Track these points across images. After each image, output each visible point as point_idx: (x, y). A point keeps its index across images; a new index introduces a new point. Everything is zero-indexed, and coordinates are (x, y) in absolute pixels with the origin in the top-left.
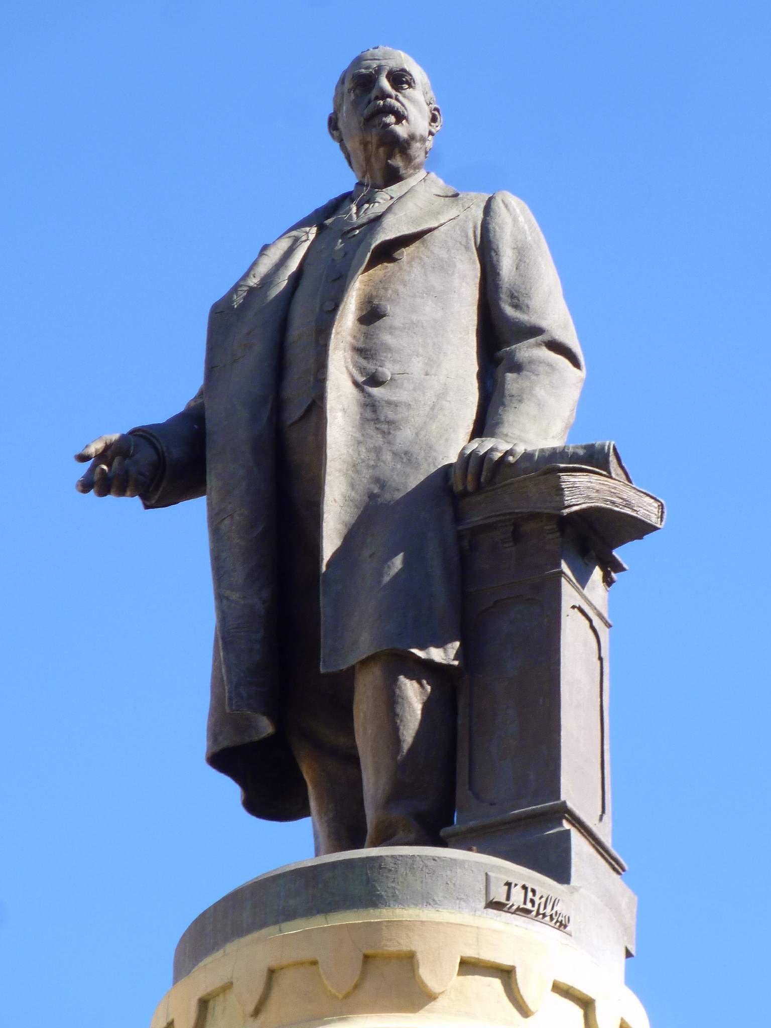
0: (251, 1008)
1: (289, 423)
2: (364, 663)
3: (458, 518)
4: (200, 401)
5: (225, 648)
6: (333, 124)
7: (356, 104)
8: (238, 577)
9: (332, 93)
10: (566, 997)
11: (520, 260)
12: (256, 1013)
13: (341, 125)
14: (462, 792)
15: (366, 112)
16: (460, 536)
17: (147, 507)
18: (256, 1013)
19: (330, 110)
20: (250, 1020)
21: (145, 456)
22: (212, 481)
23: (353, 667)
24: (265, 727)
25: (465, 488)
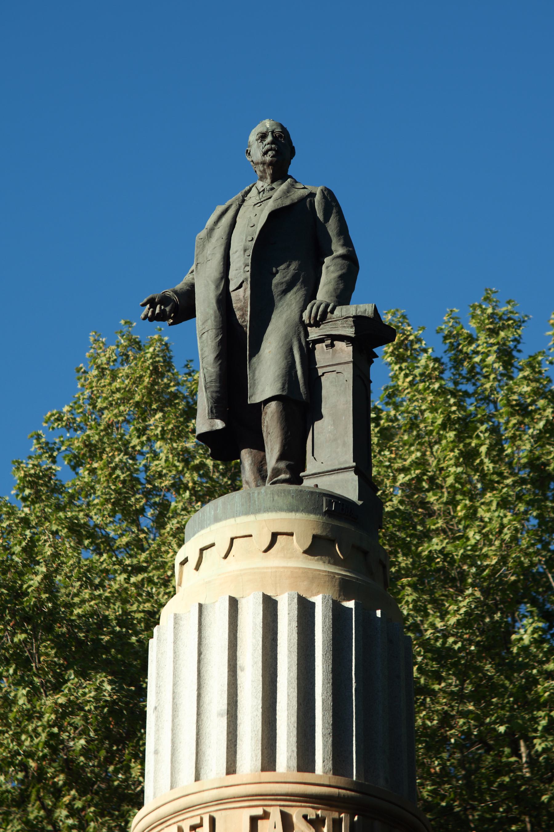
0: (223, 555)
15: (264, 150)
16: (307, 343)
18: (226, 557)
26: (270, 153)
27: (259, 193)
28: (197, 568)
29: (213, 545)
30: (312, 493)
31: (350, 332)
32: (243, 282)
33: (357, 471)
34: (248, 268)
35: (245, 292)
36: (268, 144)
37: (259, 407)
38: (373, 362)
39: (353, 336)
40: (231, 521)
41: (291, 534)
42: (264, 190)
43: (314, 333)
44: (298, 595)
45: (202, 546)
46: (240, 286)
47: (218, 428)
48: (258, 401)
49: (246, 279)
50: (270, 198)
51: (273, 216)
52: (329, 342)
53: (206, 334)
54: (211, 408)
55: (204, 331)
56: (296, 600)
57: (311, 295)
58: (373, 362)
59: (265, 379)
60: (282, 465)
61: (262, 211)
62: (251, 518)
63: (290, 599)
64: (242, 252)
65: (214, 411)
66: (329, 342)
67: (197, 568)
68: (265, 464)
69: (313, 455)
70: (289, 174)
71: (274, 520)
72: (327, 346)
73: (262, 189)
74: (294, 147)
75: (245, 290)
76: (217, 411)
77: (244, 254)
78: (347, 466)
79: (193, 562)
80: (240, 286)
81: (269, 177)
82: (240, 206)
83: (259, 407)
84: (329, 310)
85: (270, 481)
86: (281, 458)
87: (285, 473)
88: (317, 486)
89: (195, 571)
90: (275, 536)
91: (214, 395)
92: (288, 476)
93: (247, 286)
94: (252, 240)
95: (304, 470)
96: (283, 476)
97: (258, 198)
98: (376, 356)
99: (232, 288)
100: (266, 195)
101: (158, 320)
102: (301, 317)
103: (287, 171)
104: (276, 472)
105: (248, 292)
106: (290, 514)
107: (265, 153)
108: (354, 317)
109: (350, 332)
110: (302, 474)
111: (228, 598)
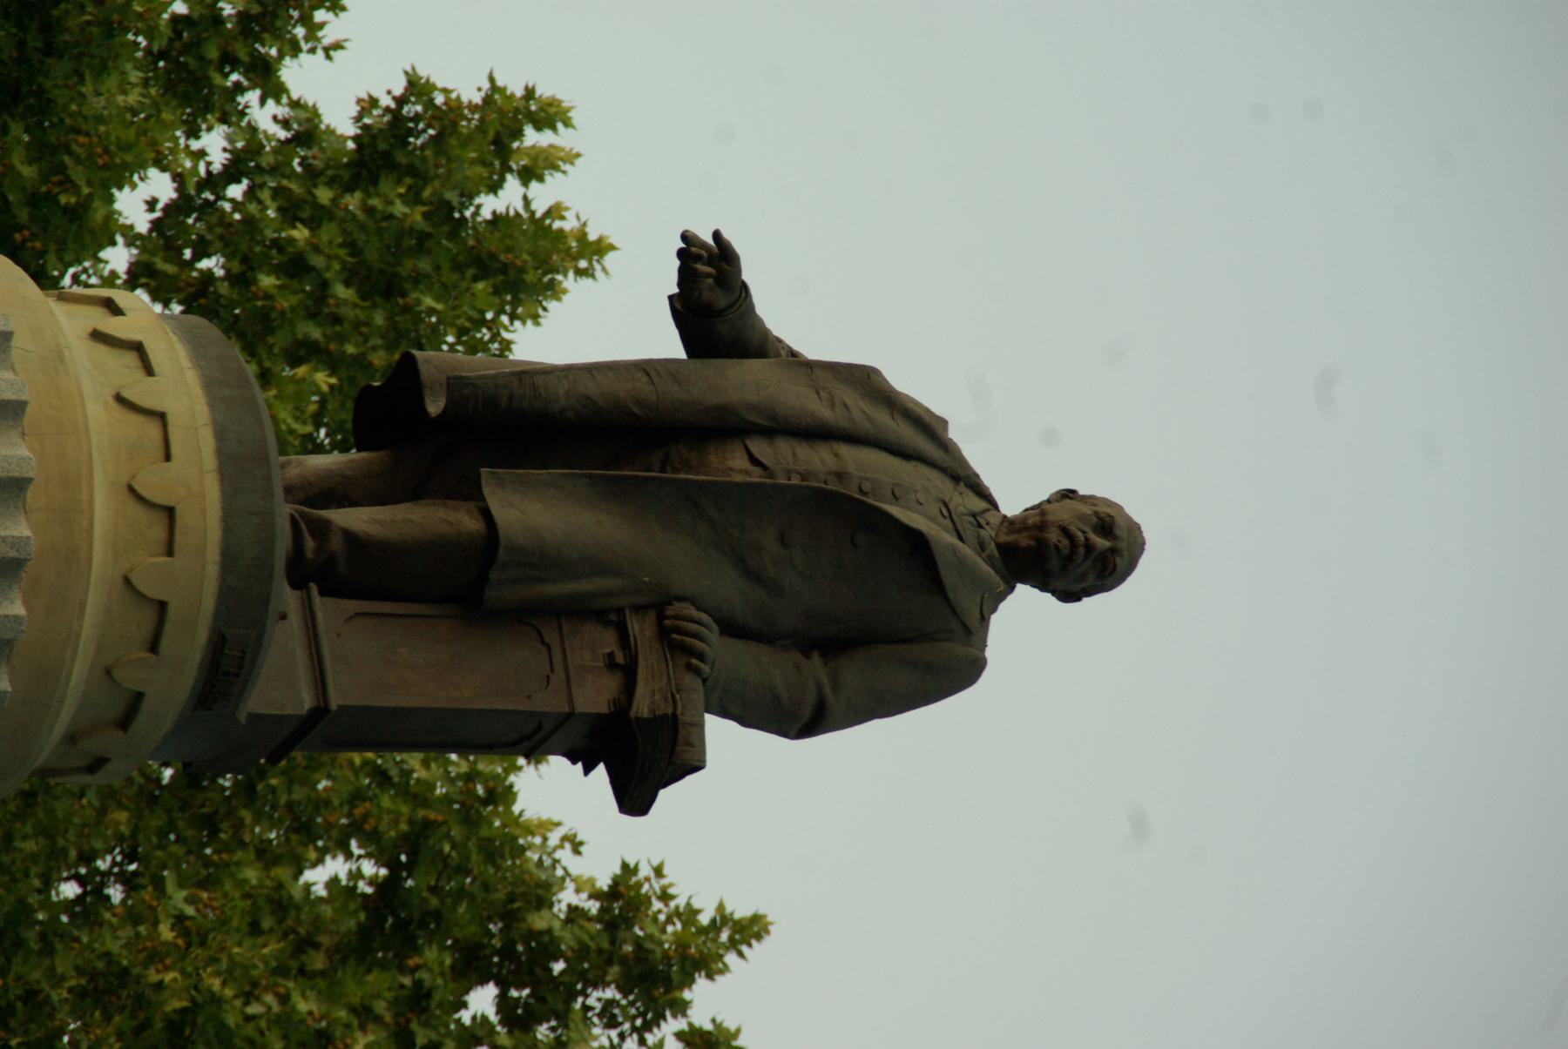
0: (126, 394)
1: (748, 442)
2: (486, 514)
3: (639, 609)
4: (783, 353)
5: (513, 374)
6: (1068, 494)
7: (1082, 518)
8: (590, 388)
9: (1099, 494)
10: (1091, 497)
11: (136, 826)
12: (120, 399)
13: (1067, 501)
14: (353, 605)
15: (1072, 528)
16: (620, 611)
17: (671, 298)
18: (120, 399)
19: (1082, 492)
20: (113, 392)
21: (720, 300)
22: (693, 361)
23: (484, 500)
24: (434, 407)
25: (666, 618)
26: (1066, 542)
27: (974, 515)
28: (97, 336)
29: (149, 371)
30: (265, 602)
31: (642, 706)
32: (765, 468)
33: (320, 712)
34: (796, 481)
35: (742, 472)
36: (1087, 539)
37: (470, 493)
38: (574, 763)
39: (632, 714)
40: (202, 411)
41: (170, 552)
42: (980, 526)
43: (641, 629)
44: (26, 560)
45: (148, 346)
46: (755, 461)
47: (427, 401)
48: (486, 490)
49: (771, 476)
50: (961, 538)
51: (917, 542)
52: (620, 659)
53: (645, 379)
54: (474, 385)
55: (653, 374)
56: (12, 554)
57: (730, 628)
58: (574, 763)
59: (531, 509)
60: (336, 543)
61: (932, 519)
62: (209, 460)
63: (17, 543)
64: (833, 468)
65: (466, 391)
66: (620, 658)
67: (97, 336)
68: (341, 505)
69: (357, 614)
70: (1020, 588)
71: (203, 513)
72: (611, 655)
73: (982, 522)
74: (1079, 599)
75: (747, 472)
76: (163, 879)
77: (830, 473)
78: (331, 691)
79: (111, 325)
80: (755, 461)
81: (1009, 539)
82: (943, 470)
83: (470, 493)
84: (694, 661)
85: (302, 514)
86: (350, 537)
87: (319, 550)
88: (283, 617)
89: (90, 330)
90: (170, 511)
91: (504, 402)
92: (309, 554)
93: (756, 476)
94: (861, 491)
95: (322, 593)
96: (310, 543)
97: (963, 510)
98: (587, 771)
99: (759, 447)
100: (969, 531)
101: (681, 271)
102: (681, 599)
103: (1023, 582)
104: (321, 530)
105: (739, 478)
106: (217, 551)
107: (1065, 531)
108: (674, 715)
109: (642, 706)
110: (314, 588)
111: (23, 398)
